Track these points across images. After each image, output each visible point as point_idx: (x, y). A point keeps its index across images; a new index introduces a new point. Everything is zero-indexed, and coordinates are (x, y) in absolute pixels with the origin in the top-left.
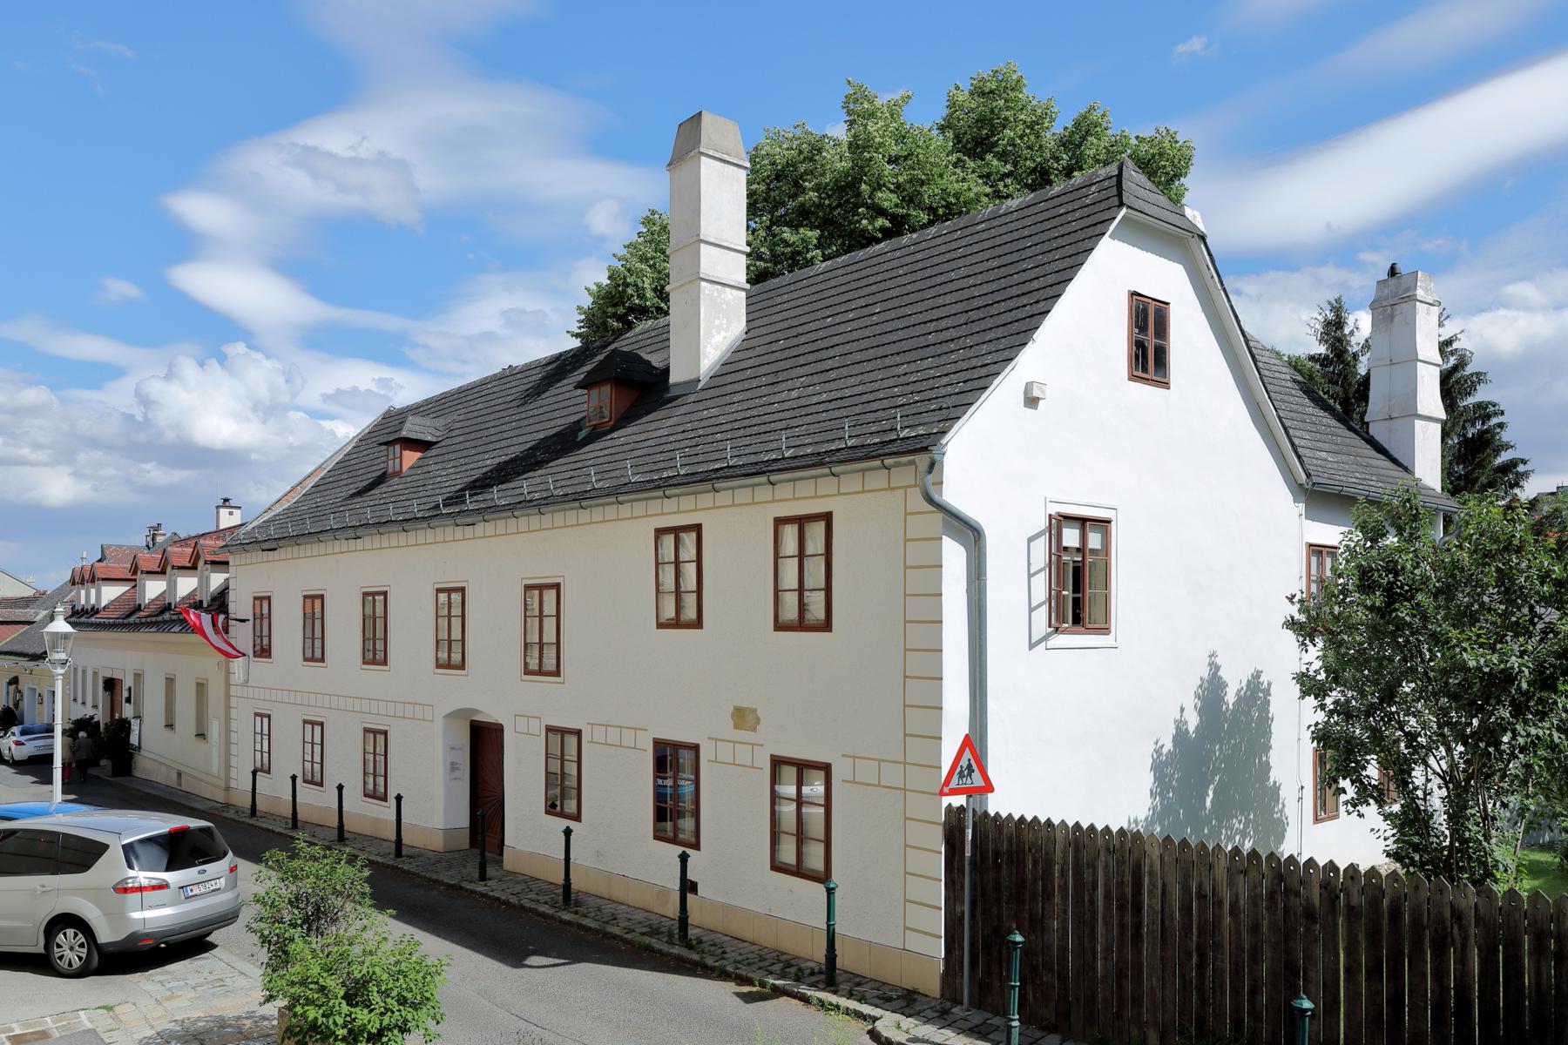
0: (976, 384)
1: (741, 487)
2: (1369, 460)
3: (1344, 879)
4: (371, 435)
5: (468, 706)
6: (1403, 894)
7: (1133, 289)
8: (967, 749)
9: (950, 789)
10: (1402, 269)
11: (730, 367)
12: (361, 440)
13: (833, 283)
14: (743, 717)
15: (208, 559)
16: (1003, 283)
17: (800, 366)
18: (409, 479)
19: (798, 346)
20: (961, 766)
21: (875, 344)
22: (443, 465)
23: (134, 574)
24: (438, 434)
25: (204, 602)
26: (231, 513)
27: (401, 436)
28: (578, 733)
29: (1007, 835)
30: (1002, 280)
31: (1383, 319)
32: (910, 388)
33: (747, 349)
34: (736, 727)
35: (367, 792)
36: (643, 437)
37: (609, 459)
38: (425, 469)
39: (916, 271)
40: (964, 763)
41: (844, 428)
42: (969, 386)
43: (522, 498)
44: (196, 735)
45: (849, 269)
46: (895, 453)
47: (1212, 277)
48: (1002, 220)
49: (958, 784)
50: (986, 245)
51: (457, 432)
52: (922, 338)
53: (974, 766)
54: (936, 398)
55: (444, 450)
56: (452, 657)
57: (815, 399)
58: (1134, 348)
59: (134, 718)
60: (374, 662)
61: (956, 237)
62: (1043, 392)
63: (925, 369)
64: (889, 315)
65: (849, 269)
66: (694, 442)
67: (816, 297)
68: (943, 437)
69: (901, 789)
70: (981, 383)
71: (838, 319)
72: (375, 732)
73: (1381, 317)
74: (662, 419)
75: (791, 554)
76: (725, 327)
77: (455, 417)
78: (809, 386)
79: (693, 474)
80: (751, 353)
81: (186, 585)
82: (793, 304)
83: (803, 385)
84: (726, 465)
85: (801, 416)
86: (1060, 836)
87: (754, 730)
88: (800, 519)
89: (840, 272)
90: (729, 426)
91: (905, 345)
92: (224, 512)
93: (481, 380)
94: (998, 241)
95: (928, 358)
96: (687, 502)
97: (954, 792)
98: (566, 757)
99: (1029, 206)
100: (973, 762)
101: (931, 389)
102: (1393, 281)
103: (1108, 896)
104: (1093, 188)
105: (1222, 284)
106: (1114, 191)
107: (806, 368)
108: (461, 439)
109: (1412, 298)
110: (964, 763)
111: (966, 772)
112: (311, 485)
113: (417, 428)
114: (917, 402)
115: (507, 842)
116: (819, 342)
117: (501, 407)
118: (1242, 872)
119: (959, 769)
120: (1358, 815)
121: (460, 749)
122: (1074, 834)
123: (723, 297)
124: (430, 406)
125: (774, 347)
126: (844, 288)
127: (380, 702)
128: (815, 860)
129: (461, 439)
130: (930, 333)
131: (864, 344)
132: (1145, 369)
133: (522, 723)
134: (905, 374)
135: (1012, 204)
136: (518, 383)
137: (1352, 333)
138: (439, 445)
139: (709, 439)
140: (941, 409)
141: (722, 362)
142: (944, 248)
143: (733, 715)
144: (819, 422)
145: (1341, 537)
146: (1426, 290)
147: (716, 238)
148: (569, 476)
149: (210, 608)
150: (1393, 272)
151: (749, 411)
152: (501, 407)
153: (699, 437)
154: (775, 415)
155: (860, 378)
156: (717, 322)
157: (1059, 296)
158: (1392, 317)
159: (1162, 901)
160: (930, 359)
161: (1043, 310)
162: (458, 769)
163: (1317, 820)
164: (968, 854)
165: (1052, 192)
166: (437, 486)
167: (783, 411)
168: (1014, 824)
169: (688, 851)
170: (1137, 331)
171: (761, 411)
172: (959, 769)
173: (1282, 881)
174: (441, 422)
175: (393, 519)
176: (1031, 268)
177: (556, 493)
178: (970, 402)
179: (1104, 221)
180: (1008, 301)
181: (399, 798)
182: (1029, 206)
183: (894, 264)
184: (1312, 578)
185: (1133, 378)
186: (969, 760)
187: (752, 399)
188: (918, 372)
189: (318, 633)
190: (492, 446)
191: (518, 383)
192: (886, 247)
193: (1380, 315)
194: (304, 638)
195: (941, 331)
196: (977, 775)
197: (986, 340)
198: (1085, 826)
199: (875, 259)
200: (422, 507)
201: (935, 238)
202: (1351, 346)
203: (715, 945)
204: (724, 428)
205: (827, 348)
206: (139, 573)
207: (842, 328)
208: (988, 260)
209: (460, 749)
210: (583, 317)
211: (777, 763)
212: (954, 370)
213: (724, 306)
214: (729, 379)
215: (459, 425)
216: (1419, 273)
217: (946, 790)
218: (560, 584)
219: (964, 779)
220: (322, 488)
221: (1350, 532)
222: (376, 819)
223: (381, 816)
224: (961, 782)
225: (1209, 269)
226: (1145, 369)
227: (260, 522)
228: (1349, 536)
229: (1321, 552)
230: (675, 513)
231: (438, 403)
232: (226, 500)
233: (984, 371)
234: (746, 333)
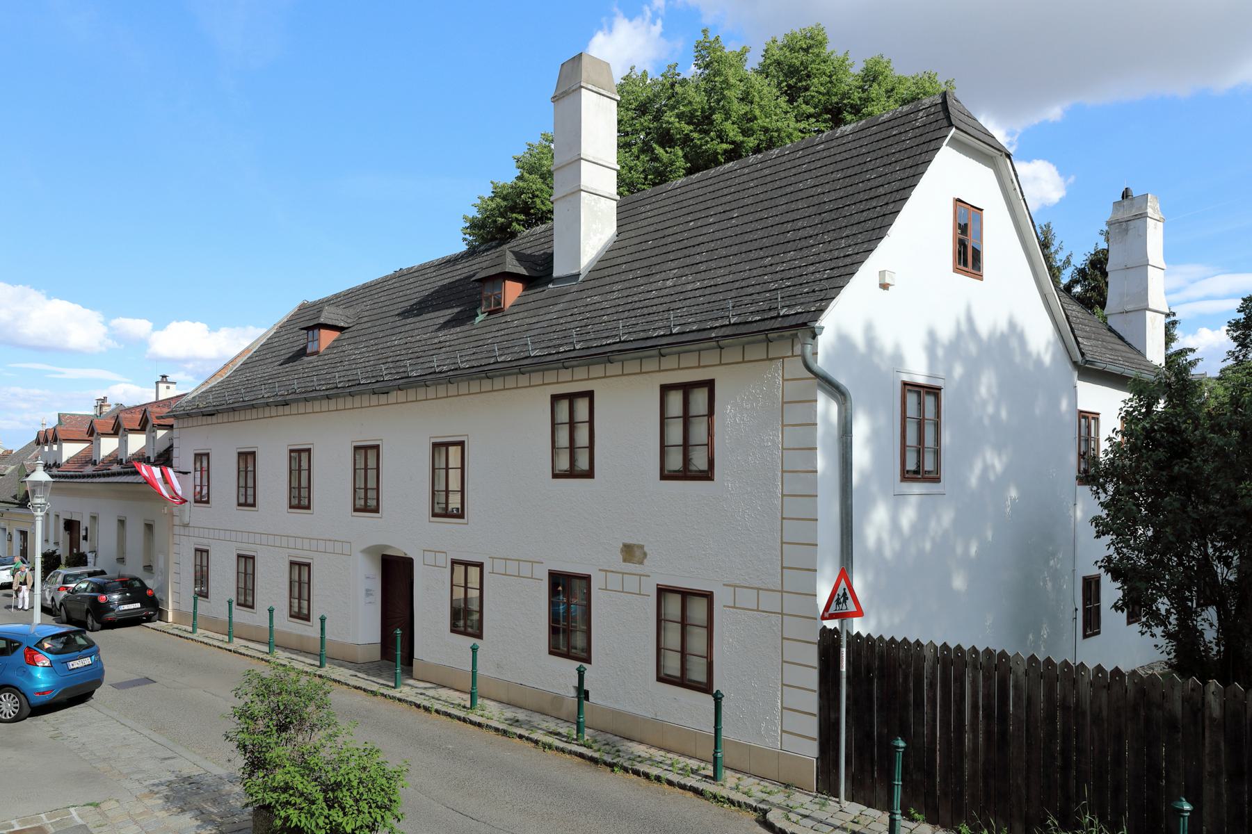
0: (842, 271)
1: (753, 342)
2: (1112, 345)
3: (1110, 679)
4: (290, 323)
5: (388, 544)
6: (910, 654)
7: (956, 197)
8: (843, 579)
9: (830, 614)
10: (1135, 192)
11: (606, 262)
12: (280, 327)
13: (690, 195)
14: (630, 552)
15: (155, 423)
16: (850, 190)
17: (671, 261)
18: (326, 357)
19: (666, 245)
20: (838, 595)
21: (738, 242)
22: (356, 345)
23: (92, 433)
24: (349, 321)
25: (151, 459)
26: (168, 388)
27: (320, 322)
28: (480, 565)
29: (878, 653)
30: (849, 188)
31: (1119, 232)
32: (779, 276)
33: (619, 249)
34: (625, 560)
35: (239, 602)
36: (534, 320)
37: (506, 338)
38: (340, 349)
39: (766, 184)
40: (840, 591)
41: (777, 299)
42: (836, 273)
43: (433, 370)
44: (117, 559)
45: (704, 183)
46: (778, 329)
47: (1015, 189)
48: (839, 141)
49: (836, 610)
50: (827, 161)
51: (366, 319)
52: (781, 236)
53: (849, 595)
54: (807, 283)
55: (355, 334)
56: (367, 502)
57: (690, 287)
58: (958, 245)
59: (90, 552)
60: (299, 507)
61: (798, 156)
62: (892, 279)
63: (790, 261)
64: (746, 219)
65: (704, 183)
66: (583, 323)
67: (676, 206)
68: (822, 313)
69: (778, 613)
70: (848, 270)
71: (699, 223)
72: (300, 565)
73: (1117, 231)
74: (550, 306)
75: (676, 415)
76: (600, 230)
77: (363, 307)
78: (682, 277)
79: (588, 348)
80: (624, 252)
81: (136, 443)
82: (656, 212)
83: (676, 275)
84: (618, 340)
85: (680, 300)
86: (928, 654)
87: (641, 563)
88: (685, 386)
89: (695, 186)
90: (614, 310)
91: (766, 242)
92: (162, 386)
93: (382, 278)
94: (838, 158)
95: (790, 252)
96: (580, 373)
97: (832, 617)
98: (469, 585)
99: (863, 130)
100: (847, 591)
101: (800, 276)
102: (1126, 202)
103: (975, 707)
104: (921, 114)
105: (1023, 196)
106: (942, 115)
107: (676, 262)
108: (369, 324)
109: (1143, 215)
110: (840, 591)
111: (842, 600)
112: (240, 363)
113: (332, 316)
114: (789, 286)
115: (416, 656)
116: (685, 241)
117: (402, 299)
118: (1105, 687)
119: (836, 597)
120: (1151, 635)
121: (373, 578)
122: (942, 653)
123: (598, 205)
124: (339, 299)
125: (644, 246)
126: (701, 199)
127: (312, 541)
128: (698, 674)
129: (369, 324)
130: (788, 232)
131: (727, 242)
132: (965, 264)
133: (430, 557)
134: (771, 265)
135: (848, 128)
136: (415, 279)
137: (1056, 252)
138: (350, 329)
139: (597, 321)
140: (814, 291)
141: (598, 259)
142: (789, 165)
143: (622, 551)
144: (698, 305)
145: (1123, 405)
146: (1154, 209)
147: (593, 157)
148: (472, 352)
149: (156, 463)
150: (1126, 195)
151: (629, 298)
152: (402, 299)
153: (588, 318)
154: (655, 300)
155: (728, 269)
156: (594, 226)
157: (907, 199)
158: (1127, 230)
159: (1027, 712)
160: (792, 253)
161: (893, 210)
162: (371, 595)
163: (1085, 636)
164: (844, 669)
165: (882, 118)
166: (352, 362)
167: (662, 297)
168: (885, 645)
169: (585, 665)
170: (959, 231)
171: (641, 297)
172: (836, 597)
173: (1041, 678)
174: (351, 312)
175: (318, 388)
176: (875, 178)
177: (462, 366)
178: (841, 285)
179: (937, 139)
180: (858, 205)
181: (323, 620)
182: (863, 130)
183: (745, 178)
184: (1082, 438)
185: (956, 270)
186: (844, 589)
187: (630, 288)
188: (783, 262)
189: (250, 483)
190: (397, 330)
191: (415, 279)
192: (735, 165)
193: (1116, 229)
194: (238, 487)
195: (799, 230)
196: (850, 602)
197: (843, 235)
198: (952, 646)
199: (726, 175)
200: (342, 379)
201: (779, 157)
202: (1056, 262)
203: (607, 744)
204: (609, 311)
205: (694, 246)
206: (95, 435)
207: (704, 230)
208: (832, 173)
209: (373, 578)
210: (468, 225)
211: (662, 591)
212: (817, 260)
213: (600, 213)
214: (606, 272)
215: (366, 314)
216: (1149, 195)
217: (826, 615)
218: (464, 441)
219: (841, 606)
220: (250, 365)
221: (1131, 400)
222: (301, 636)
223: (304, 634)
224: (838, 608)
225: (1013, 182)
226: (965, 264)
227: (199, 392)
228: (1130, 404)
229: (1088, 417)
230: (570, 382)
231: (347, 297)
232: (164, 377)
233: (848, 260)
234: (617, 236)
